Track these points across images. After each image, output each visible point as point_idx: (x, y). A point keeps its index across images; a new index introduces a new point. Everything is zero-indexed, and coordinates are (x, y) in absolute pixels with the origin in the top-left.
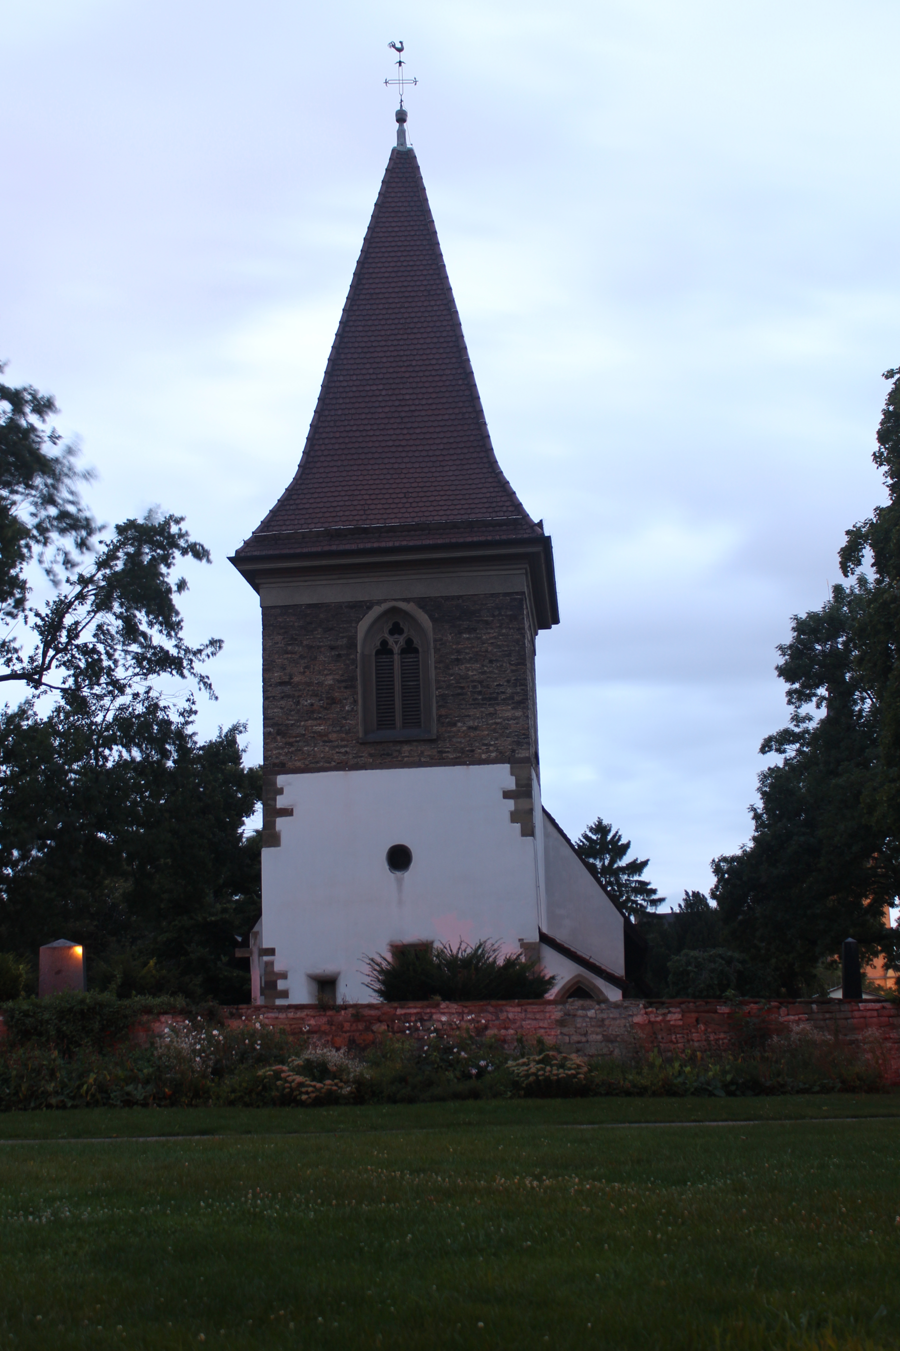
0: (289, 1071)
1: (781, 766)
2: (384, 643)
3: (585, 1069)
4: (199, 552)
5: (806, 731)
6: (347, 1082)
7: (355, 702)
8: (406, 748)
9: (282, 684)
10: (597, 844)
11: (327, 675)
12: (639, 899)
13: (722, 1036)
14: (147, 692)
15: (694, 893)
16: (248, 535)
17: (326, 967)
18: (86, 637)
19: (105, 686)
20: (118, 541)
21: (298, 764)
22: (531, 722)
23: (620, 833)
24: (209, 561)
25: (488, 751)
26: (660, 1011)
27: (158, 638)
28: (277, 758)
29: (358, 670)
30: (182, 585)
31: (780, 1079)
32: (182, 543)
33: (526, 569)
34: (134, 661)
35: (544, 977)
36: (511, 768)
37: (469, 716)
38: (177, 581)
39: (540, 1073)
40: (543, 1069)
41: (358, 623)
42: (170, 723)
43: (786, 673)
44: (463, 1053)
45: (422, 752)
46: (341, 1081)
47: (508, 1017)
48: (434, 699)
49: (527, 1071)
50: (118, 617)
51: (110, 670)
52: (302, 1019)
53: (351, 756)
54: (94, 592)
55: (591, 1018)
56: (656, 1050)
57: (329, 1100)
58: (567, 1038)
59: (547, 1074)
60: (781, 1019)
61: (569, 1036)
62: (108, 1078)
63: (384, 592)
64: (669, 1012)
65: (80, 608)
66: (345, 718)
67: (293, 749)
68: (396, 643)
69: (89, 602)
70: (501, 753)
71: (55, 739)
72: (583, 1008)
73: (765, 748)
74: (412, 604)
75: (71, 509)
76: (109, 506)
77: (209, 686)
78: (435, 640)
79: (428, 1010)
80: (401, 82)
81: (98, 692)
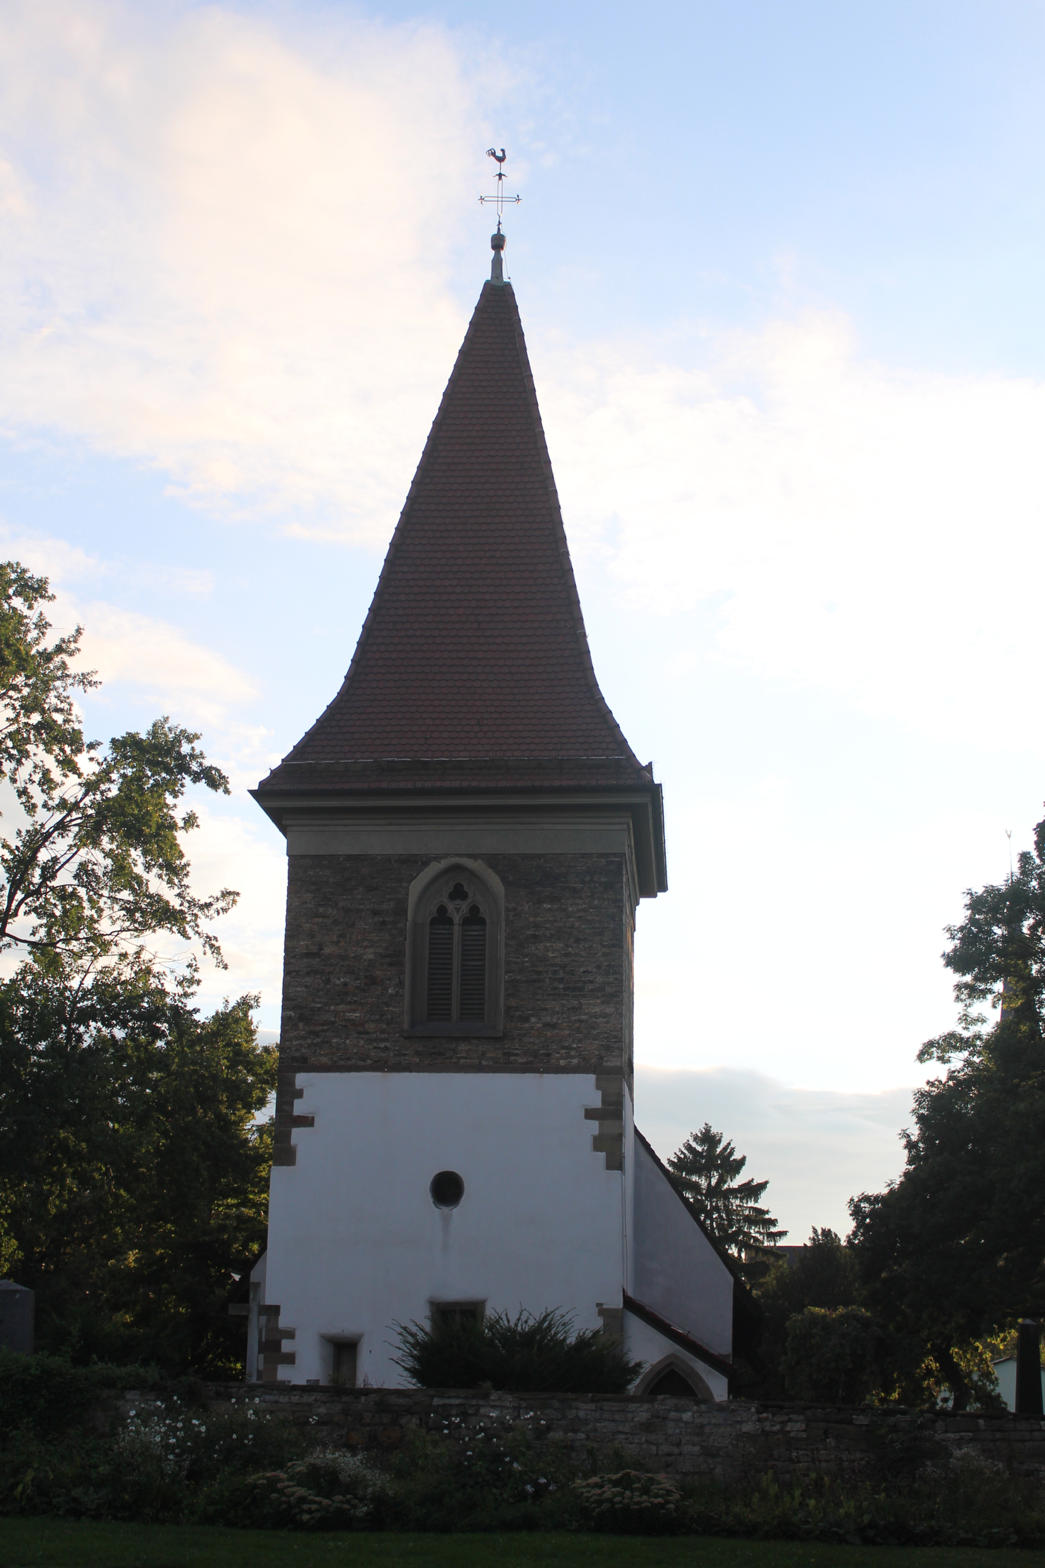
0: (288, 1480)
1: (944, 1080)
2: (442, 910)
3: (676, 1496)
4: (214, 779)
5: (978, 1037)
6: (362, 1500)
7: (401, 983)
8: (463, 1047)
9: (308, 955)
10: (703, 1157)
11: (366, 947)
12: (753, 1231)
13: (858, 1455)
14: (138, 954)
15: (823, 1230)
16: (277, 763)
17: (344, 1327)
18: (64, 878)
19: (84, 941)
20: (114, 759)
21: (324, 1060)
22: (625, 1022)
23: (732, 1146)
24: (227, 791)
25: (568, 1056)
26: (779, 1418)
27: (156, 884)
28: (297, 1050)
29: (407, 942)
30: (190, 821)
31: (934, 1523)
32: (194, 767)
33: (628, 825)
34: (124, 912)
35: (628, 1363)
36: (597, 1080)
37: (546, 1009)
38: (185, 815)
39: (617, 1499)
40: (622, 1494)
41: (410, 882)
42: (163, 993)
43: (957, 961)
44: (515, 1465)
45: (484, 1053)
46: (355, 1497)
47: (577, 1417)
48: (503, 986)
49: (600, 1495)
50: (107, 854)
51: (93, 921)
52: (310, 1405)
53: (392, 1054)
54: (79, 821)
55: (686, 1423)
56: (771, 1472)
57: (335, 1522)
58: (654, 1448)
59: (626, 1501)
60: (938, 1437)
61: (657, 1445)
62: (52, 1476)
63: (443, 842)
64: (790, 1420)
65: (59, 840)
66: (387, 1004)
67: (318, 1040)
68: (458, 910)
69: (71, 835)
70: (584, 1059)
71: (18, 1008)
72: (677, 1409)
73: (923, 1055)
74: (480, 861)
75: (58, 718)
76: (103, 715)
77: (216, 950)
78: (507, 910)
79: (474, 1402)
80: (501, 200)
81: (76, 949)
